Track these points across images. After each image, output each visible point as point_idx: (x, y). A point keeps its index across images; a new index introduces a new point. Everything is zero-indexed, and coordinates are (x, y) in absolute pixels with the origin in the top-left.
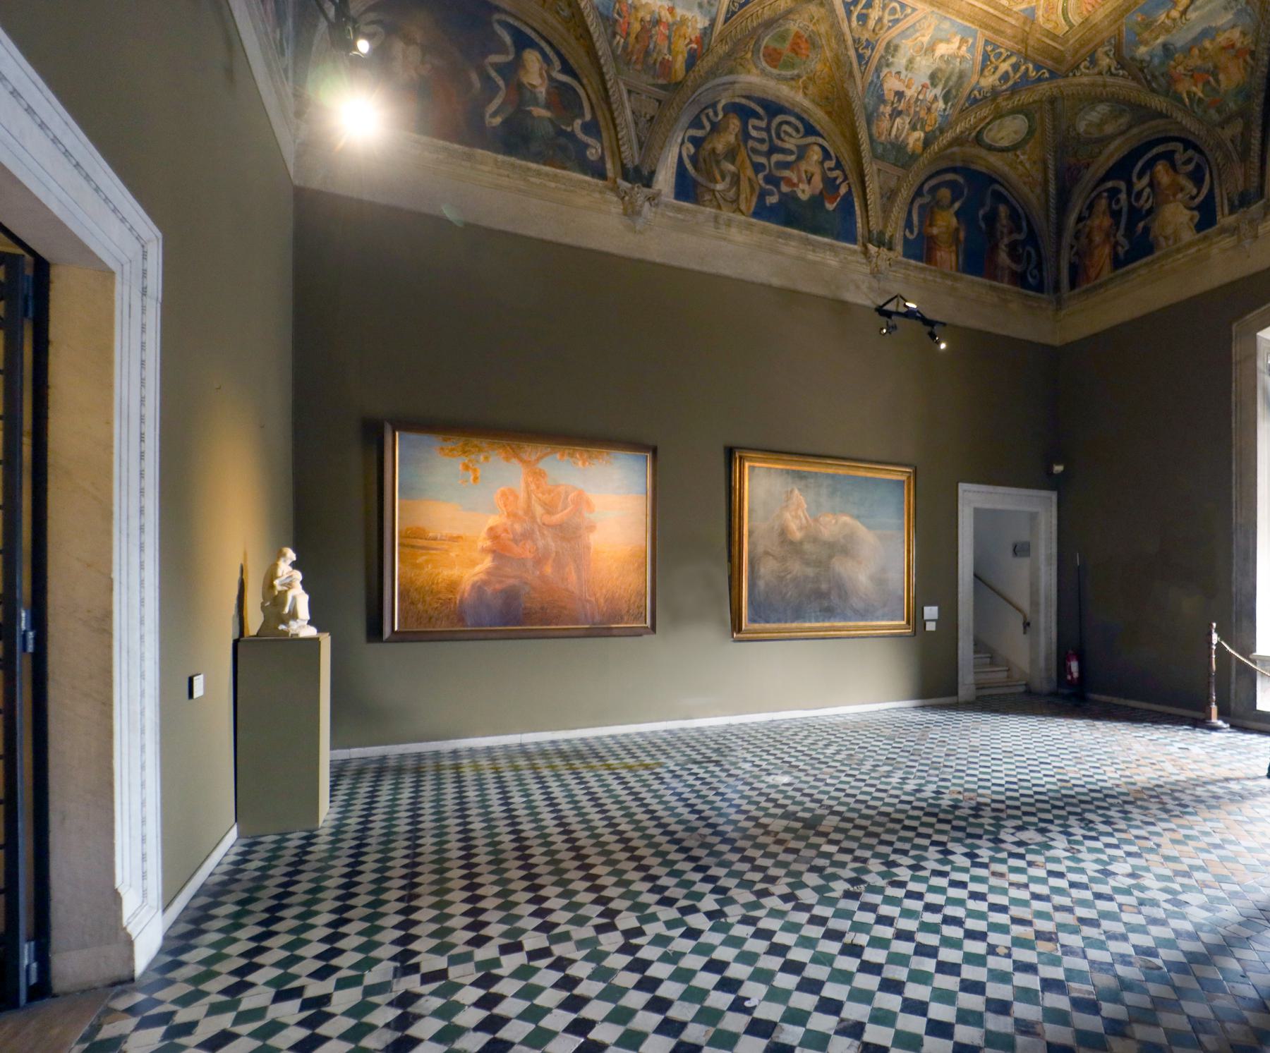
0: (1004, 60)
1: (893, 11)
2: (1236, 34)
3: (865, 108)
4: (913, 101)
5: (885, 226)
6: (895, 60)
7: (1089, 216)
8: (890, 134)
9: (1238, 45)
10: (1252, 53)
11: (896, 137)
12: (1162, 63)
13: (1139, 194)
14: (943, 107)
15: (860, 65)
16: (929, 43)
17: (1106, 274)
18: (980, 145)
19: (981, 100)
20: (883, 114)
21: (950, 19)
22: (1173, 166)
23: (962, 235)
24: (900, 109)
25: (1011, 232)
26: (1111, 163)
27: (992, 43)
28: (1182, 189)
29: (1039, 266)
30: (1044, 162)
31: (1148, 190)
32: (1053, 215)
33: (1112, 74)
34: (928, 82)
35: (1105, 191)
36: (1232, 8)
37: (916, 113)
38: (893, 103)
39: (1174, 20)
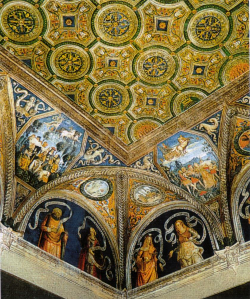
0: (98, 150)
1: (41, 106)
2: (209, 163)
3: (16, 148)
4: (45, 154)
5: (15, 215)
6: (38, 131)
7: (142, 246)
8: (29, 167)
9: (211, 168)
10: (218, 173)
12: (176, 171)
13: (169, 236)
14: (63, 163)
15: (17, 126)
16: (59, 128)
17: (154, 279)
18: (82, 194)
19: (84, 166)
21: (71, 120)
22: (185, 223)
23: (66, 237)
24: (37, 155)
25: (97, 245)
26: (153, 219)
27: (92, 139)
28: (192, 235)
29: (113, 270)
30: (117, 210)
31: (173, 234)
32: (122, 242)
33: (152, 171)
34: (56, 148)
35: (150, 233)
36: (206, 151)
39: (180, 151)
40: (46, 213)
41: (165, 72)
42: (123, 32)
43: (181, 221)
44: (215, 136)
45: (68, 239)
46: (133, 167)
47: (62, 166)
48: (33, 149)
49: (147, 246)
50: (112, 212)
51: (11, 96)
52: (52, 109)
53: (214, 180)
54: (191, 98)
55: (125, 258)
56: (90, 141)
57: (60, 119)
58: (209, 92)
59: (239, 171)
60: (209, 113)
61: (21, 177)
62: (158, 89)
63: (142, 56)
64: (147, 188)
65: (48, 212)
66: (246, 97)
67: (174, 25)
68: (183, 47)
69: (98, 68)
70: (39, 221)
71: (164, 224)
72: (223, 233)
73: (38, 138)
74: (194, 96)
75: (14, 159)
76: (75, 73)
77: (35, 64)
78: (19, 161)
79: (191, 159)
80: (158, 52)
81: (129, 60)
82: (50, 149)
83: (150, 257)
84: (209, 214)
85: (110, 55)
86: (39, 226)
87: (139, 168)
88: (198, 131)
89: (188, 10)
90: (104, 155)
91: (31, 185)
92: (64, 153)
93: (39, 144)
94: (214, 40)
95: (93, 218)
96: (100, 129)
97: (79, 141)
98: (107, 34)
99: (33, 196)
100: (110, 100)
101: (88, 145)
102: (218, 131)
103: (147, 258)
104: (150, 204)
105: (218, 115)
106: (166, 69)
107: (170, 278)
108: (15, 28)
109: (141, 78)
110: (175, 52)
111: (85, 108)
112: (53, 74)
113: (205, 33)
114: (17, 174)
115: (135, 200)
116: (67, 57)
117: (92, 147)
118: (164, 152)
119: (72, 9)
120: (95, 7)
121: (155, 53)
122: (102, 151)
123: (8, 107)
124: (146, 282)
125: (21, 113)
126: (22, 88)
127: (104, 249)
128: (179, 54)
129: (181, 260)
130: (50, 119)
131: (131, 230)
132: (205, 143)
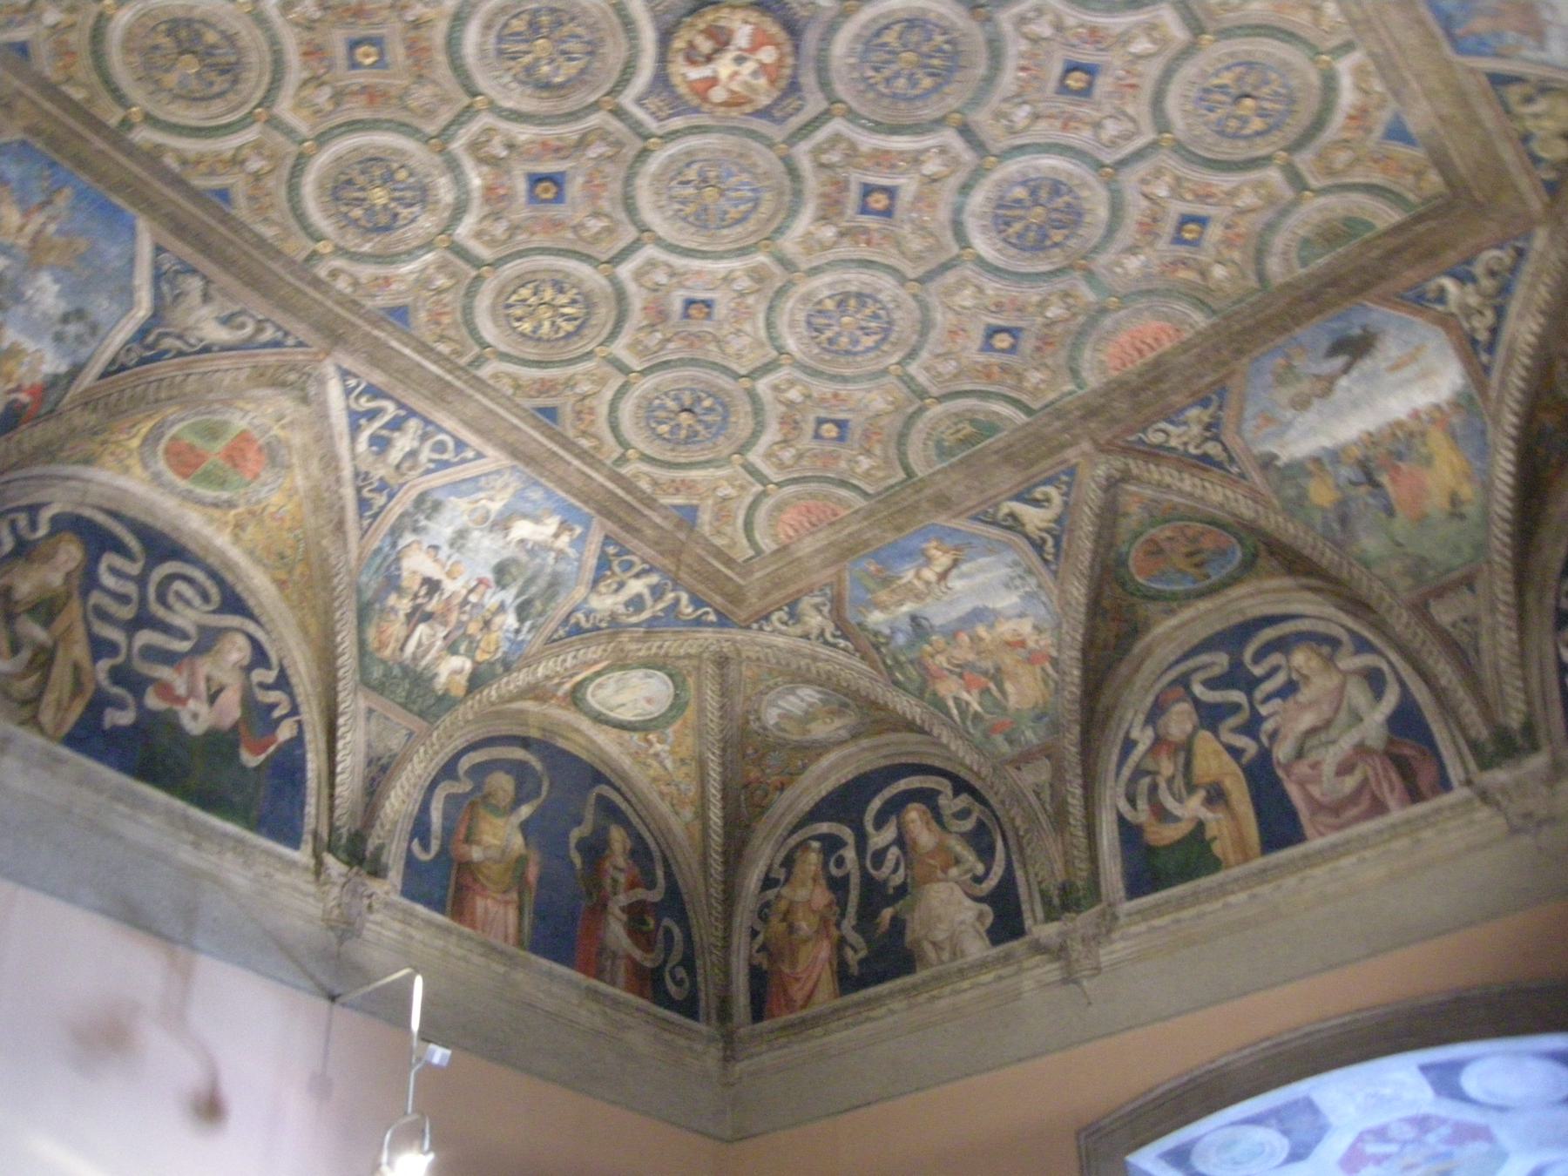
0: (637, 576)
1: (440, 447)
2: (1026, 627)
3: (359, 591)
8: (402, 649)
10: (1055, 662)
11: (415, 658)
12: (911, 645)
13: (880, 857)
14: (516, 625)
15: (361, 516)
16: (501, 513)
19: (588, 631)
20: (393, 609)
22: (937, 814)
23: (533, 873)
24: (429, 608)
25: (632, 885)
27: (616, 544)
28: (958, 861)
29: (688, 962)
31: (894, 852)
32: (716, 867)
33: (826, 643)
34: (490, 576)
36: (1017, 588)
37: (461, 624)
38: (416, 596)
39: (928, 583)
40: (465, 795)
41: (884, 340)
42: (737, 216)
43: (923, 807)
44: (1050, 542)
45: (540, 879)
46: (761, 629)
47: (511, 636)
48: (416, 587)
49: (803, 884)
50: (685, 769)
51: (339, 420)
52: (480, 455)
53: (1041, 685)
54: (972, 421)
55: (728, 917)
56: (611, 550)
57: (506, 486)
58: (1036, 405)
59: (1127, 651)
60: (1035, 469)
61: (380, 688)
62: (856, 392)
63: (801, 289)
64: (809, 694)
65: (472, 791)
66: (1163, 425)
67: (918, 198)
68: (945, 267)
69: (645, 323)
70: (444, 828)
71: (862, 812)
72: (1059, 865)
73: (432, 552)
74: (980, 417)
75: (354, 631)
76: (562, 343)
77: (423, 316)
78: (371, 634)
79: (965, 607)
80: (856, 280)
81: (757, 301)
82: (473, 583)
83: (815, 920)
84: (1017, 797)
85: (688, 283)
86: (443, 850)
87: (782, 633)
88: (994, 523)
89: (968, 156)
90: (657, 592)
91: (411, 711)
92: (517, 596)
93: (434, 572)
94: (1057, 250)
95: (618, 790)
96: (647, 512)
97: (572, 552)
98: (681, 224)
99: (422, 750)
100: (685, 424)
101: (604, 564)
102: (1061, 529)
103: (804, 925)
104: (814, 742)
105: (1064, 478)
106: (886, 331)
107: (878, 1000)
108: (357, 212)
109: (798, 355)
110: (920, 281)
111: (595, 448)
112: (484, 345)
113: (1027, 228)
114: (365, 682)
115: (765, 729)
116: (535, 294)
117: (617, 569)
118: (872, 585)
119: (558, 150)
120: (639, 144)
121: (847, 281)
122: (654, 579)
123: (330, 462)
124: (800, 1003)
125: (373, 473)
126: (374, 392)
127: (655, 896)
128: (933, 286)
129: (917, 942)
130: (471, 485)
131: (748, 826)
132: (1016, 564)
